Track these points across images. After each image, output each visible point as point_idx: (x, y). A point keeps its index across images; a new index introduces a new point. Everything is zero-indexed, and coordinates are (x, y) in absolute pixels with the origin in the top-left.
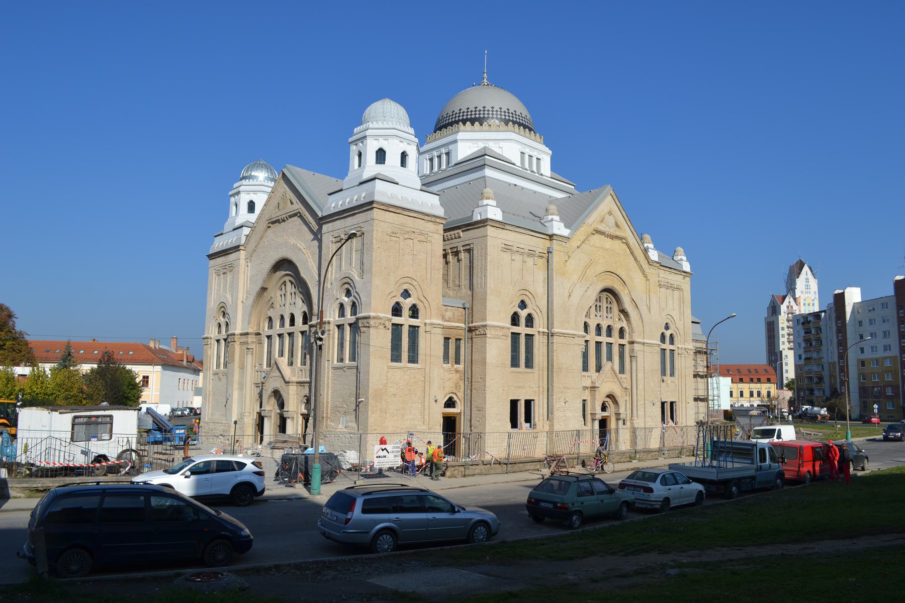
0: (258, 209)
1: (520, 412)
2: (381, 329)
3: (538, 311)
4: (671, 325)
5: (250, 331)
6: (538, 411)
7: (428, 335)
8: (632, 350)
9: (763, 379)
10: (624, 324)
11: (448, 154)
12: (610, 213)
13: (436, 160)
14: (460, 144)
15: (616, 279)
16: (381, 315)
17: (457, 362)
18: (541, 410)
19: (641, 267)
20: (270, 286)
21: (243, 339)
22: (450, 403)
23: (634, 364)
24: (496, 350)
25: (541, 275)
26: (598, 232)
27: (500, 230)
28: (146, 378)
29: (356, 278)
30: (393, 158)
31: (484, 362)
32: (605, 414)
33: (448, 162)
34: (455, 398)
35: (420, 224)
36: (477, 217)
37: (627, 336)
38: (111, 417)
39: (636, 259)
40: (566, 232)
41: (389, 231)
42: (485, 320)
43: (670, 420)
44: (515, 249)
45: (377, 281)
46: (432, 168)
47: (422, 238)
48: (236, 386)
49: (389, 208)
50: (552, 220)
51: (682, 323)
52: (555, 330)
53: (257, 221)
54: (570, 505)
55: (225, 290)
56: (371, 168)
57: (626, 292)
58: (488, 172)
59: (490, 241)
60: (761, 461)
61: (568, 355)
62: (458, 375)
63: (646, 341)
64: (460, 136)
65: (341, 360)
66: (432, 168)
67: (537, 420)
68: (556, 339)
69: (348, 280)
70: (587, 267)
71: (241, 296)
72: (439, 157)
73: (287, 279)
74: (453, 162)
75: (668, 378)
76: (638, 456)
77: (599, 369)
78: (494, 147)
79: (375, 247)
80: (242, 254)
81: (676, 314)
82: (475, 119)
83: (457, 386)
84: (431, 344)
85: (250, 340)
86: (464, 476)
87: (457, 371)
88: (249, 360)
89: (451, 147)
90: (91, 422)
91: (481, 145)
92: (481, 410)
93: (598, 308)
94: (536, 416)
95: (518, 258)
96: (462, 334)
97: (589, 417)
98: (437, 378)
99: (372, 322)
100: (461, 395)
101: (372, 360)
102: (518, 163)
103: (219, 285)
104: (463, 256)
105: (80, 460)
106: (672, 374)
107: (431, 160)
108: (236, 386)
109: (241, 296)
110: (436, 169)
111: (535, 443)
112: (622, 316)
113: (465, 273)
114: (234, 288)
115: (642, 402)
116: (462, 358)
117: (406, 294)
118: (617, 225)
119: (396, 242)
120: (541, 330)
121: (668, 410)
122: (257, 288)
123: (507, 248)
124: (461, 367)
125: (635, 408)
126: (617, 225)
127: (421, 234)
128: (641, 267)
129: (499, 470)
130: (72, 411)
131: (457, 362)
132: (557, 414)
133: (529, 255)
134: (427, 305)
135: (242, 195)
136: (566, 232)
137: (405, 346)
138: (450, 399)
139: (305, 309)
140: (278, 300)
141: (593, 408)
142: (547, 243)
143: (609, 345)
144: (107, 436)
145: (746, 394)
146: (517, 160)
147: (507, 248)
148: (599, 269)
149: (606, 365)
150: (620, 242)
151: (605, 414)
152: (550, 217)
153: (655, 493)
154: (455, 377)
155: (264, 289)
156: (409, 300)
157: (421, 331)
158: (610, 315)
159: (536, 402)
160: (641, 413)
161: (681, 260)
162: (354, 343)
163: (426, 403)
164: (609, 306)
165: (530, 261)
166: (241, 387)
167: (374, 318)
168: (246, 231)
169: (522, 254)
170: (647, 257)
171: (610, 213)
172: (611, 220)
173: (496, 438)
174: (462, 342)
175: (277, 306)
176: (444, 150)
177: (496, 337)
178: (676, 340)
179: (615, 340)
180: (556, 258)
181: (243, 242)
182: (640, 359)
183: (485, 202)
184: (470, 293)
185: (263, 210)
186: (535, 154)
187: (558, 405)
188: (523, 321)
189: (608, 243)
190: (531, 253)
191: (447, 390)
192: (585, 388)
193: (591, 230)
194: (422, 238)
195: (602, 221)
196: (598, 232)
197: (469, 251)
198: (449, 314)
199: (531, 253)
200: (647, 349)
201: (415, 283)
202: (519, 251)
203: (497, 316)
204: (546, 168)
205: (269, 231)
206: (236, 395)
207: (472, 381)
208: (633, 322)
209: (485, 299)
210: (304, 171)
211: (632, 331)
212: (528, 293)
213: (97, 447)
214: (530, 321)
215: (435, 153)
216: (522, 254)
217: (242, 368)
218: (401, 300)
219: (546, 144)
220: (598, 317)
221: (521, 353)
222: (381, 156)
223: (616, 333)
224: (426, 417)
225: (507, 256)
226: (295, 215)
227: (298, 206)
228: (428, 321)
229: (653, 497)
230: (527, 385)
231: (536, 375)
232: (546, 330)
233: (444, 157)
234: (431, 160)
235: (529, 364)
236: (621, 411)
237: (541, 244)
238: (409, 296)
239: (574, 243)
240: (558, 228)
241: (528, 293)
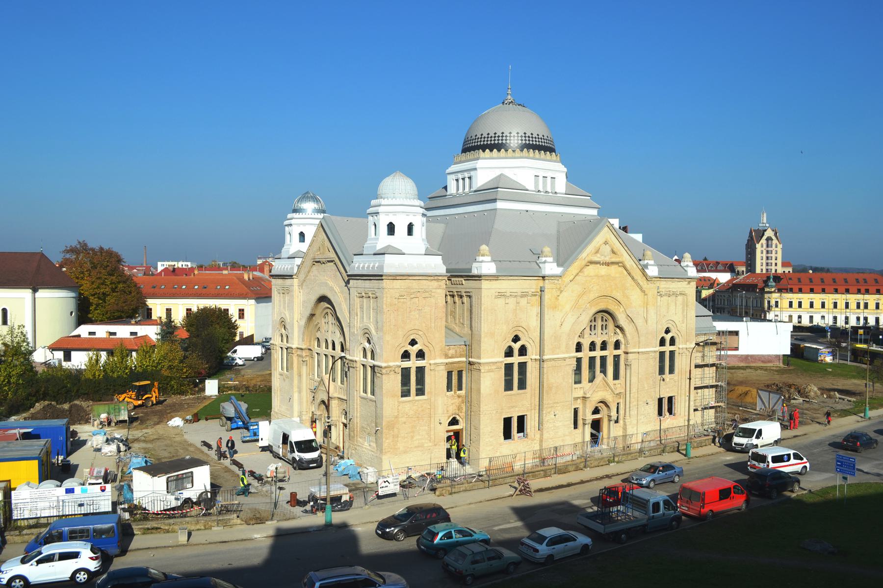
0: (308, 238)
1: (512, 427)
2: (392, 376)
3: (531, 342)
4: (672, 328)
5: (303, 347)
6: (530, 424)
7: (432, 373)
8: (626, 360)
9: (872, 289)
10: (620, 337)
11: (470, 178)
12: (606, 243)
13: (461, 181)
14: (479, 171)
15: (610, 300)
16: (391, 364)
17: (460, 388)
18: (533, 422)
19: (638, 284)
20: (318, 312)
21: (299, 352)
22: (454, 422)
23: (628, 371)
24: (490, 381)
25: (536, 310)
26: (591, 262)
27: (494, 282)
28: (241, 313)
29: (373, 332)
30: (401, 229)
31: (479, 390)
32: (597, 416)
33: (470, 187)
34: (458, 418)
35: (425, 284)
36: (475, 272)
37: (622, 346)
38: (192, 473)
39: (633, 278)
40: (558, 271)
41: (397, 295)
42: (479, 358)
43: (667, 414)
44: (508, 294)
45: (388, 338)
46: (458, 189)
47: (427, 295)
48: (295, 389)
49: (395, 277)
50: (545, 262)
51: (684, 325)
52: (545, 357)
53: (308, 250)
54: (464, 572)
55: (284, 308)
56: (383, 240)
57: (622, 309)
58: (500, 205)
59: (484, 293)
60: (654, 512)
61: (560, 375)
62: (460, 399)
63: (640, 350)
64: (480, 164)
65: (365, 391)
66: (458, 189)
67: (529, 431)
68: (545, 365)
69: (366, 331)
70: (580, 296)
71: (296, 316)
72: (463, 179)
73: (329, 311)
74: (474, 189)
75: (667, 376)
76: (616, 459)
77: (591, 380)
78: (508, 173)
79: (385, 310)
80: (295, 281)
81: (678, 319)
82: (495, 145)
83: (459, 408)
84: (435, 380)
85: (304, 354)
86: (451, 494)
87: (459, 396)
88: (304, 370)
89: (472, 173)
90: (179, 479)
91: (497, 173)
92: (477, 428)
93: (592, 328)
94: (529, 427)
95: (512, 300)
96: (464, 367)
97: (580, 422)
98: (441, 402)
99: (384, 371)
100: (463, 414)
101: (385, 399)
103: (280, 301)
104: (465, 299)
105: (174, 504)
106: (672, 371)
107: (457, 180)
108: (295, 389)
109: (296, 316)
110: (461, 190)
111: (520, 452)
112: (618, 330)
113: (467, 314)
114: (291, 309)
115: (635, 403)
116: (464, 386)
117: (413, 343)
118: (613, 252)
119: (404, 303)
120: (534, 357)
121: (666, 406)
122: (308, 313)
123: (501, 295)
124: (463, 392)
125: (627, 410)
126: (613, 252)
127: (426, 292)
128: (638, 284)
129: (482, 486)
130: (166, 473)
131: (460, 388)
132: (546, 425)
133: (522, 296)
134: (432, 349)
135: (294, 227)
136: (558, 271)
137: (413, 382)
138: (454, 418)
139: (342, 340)
140: (324, 327)
141: (584, 414)
142: (541, 283)
143: (603, 359)
144: (189, 485)
145: (853, 306)
146: (531, 186)
147: (501, 295)
148: (592, 296)
149: (599, 375)
150: (616, 266)
151: (597, 416)
152: (544, 259)
153: (541, 553)
154: (457, 401)
155: (312, 315)
156: (416, 346)
157: (427, 370)
158: (605, 331)
159: (529, 417)
160: (634, 412)
161: (687, 266)
162: (373, 382)
163: (432, 426)
164: (604, 323)
165: (523, 301)
166: (300, 392)
167: (385, 367)
168: (298, 261)
169: (516, 296)
170: (645, 275)
171: (606, 243)
172: (607, 249)
173: (490, 448)
174: (464, 373)
175: (322, 330)
176: (466, 175)
177: (489, 371)
178: (677, 341)
179: (610, 353)
180: (547, 296)
181: (295, 271)
182: (634, 367)
183: (481, 258)
184: (470, 332)
185: (313, 241)
186: (549, 175)
187: (548, 417)
188: (516, 352)
189: (603, 270)
190: (524, 295)
191: (451, 412)
192: (576, 399)
193: (584, 263)
194: (427, 295)
195: (597, 252)
196: (591, 262)
197: (470, 297)
198: (452, 352)
199: (524, 295)
200: (641, 356)
201: (420, 333)
202: (513, 295)
203: (491, 356)
204: (561, 185)
205: (314, 268)
206: (296, 396)
207: (471, 404)
208: (628, 335)
209: (480, 341)
210: (339, 218)
211: (627, 343)
212: (521, 329)
213: (186, 494)
214: (523, 351)
215: (460, 176)
216: (516, 296)
217: (300, 375)
218: (409, 348)
219: (563, 162)
220: (593, 336)
221: (515, 377)
222: (391, 229)
223: (611, 346)
224: (432, 436)
225: (501, 301)
226: (332, 261)
227: (332, 255)
228: (432, 362)
229: (538, 556)
230: (519, 403)
231: (528, 395)
232: (538, 357)
233: (467, 180)
234: (457, 180)
235: (522, 385)
236: (612, 414)
237: (532, 285)
238: (416, 343)
239: (567, 279)
240: (550, 268)
241: (521, 329)
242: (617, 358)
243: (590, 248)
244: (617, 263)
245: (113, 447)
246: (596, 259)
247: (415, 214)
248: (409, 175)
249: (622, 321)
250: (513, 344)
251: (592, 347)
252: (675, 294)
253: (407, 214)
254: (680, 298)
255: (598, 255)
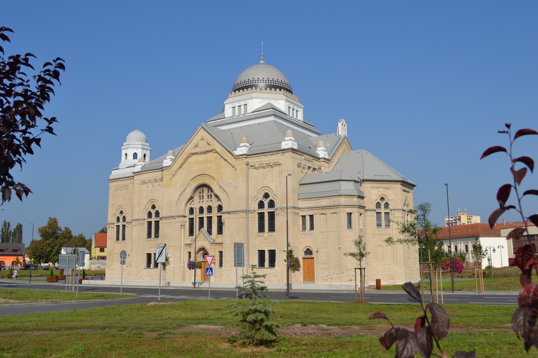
12: (202, 139)
47: (126, 188)
81: (273, 185)
95: (150, 185)
102: (288, 114)
118: (209, 144)
123: (144, 182)
126: (209, 144)
143: (210, 219)
147: (144, 182)
150: (212, 153)
171: (202, 139)
189: (203, 157)
194: (126, 188)
202: (150, 182)
223: (205, 211)
225: (145, 186)
235: (272, 228)
242: (220, 218)
243: (191, 145)
244: (212, 151)
245: (447, 226)
246: (195, 151)
247: (137, 148)
248: (141, 131)
249: (216, 190)
250: (381, 202)
251: (201, 210)
252: (269, 165)
253: (133, 148)
254: (276, 168)
255: (197, 148)
